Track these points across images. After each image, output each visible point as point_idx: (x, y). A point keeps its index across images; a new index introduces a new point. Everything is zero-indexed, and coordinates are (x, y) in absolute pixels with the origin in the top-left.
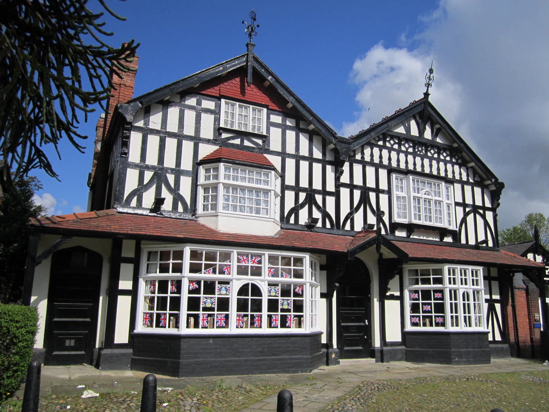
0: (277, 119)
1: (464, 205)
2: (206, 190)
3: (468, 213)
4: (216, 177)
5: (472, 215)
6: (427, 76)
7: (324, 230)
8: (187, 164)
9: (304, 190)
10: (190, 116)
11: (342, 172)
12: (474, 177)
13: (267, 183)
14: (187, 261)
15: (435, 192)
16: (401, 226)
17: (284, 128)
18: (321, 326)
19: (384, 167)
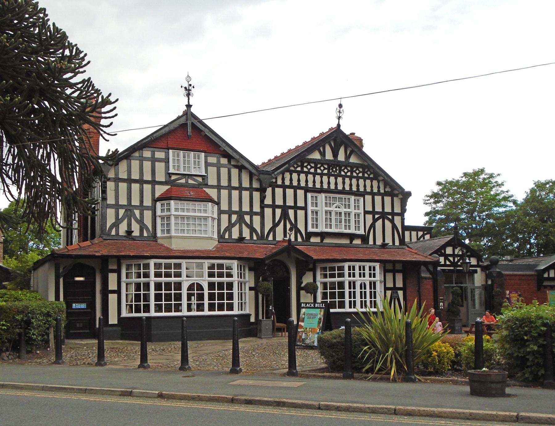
0: (212, 160)
1: (373, 213)
2: (162, 218)
3: (378, 219)
4: (169, 210)
5: (380, 222)
6: (338, 110)
7: (253, 242)
8: (148, 202)
9: (235, 212)
10: (147, 165)
11: (265, 197)
12: (385, 188)
13: (205, 211)
14: (152, 271)
15: (345, 205)
16: (316, 234)
17: (219, 166)
18: (249, 309)
19: (301, 188)
